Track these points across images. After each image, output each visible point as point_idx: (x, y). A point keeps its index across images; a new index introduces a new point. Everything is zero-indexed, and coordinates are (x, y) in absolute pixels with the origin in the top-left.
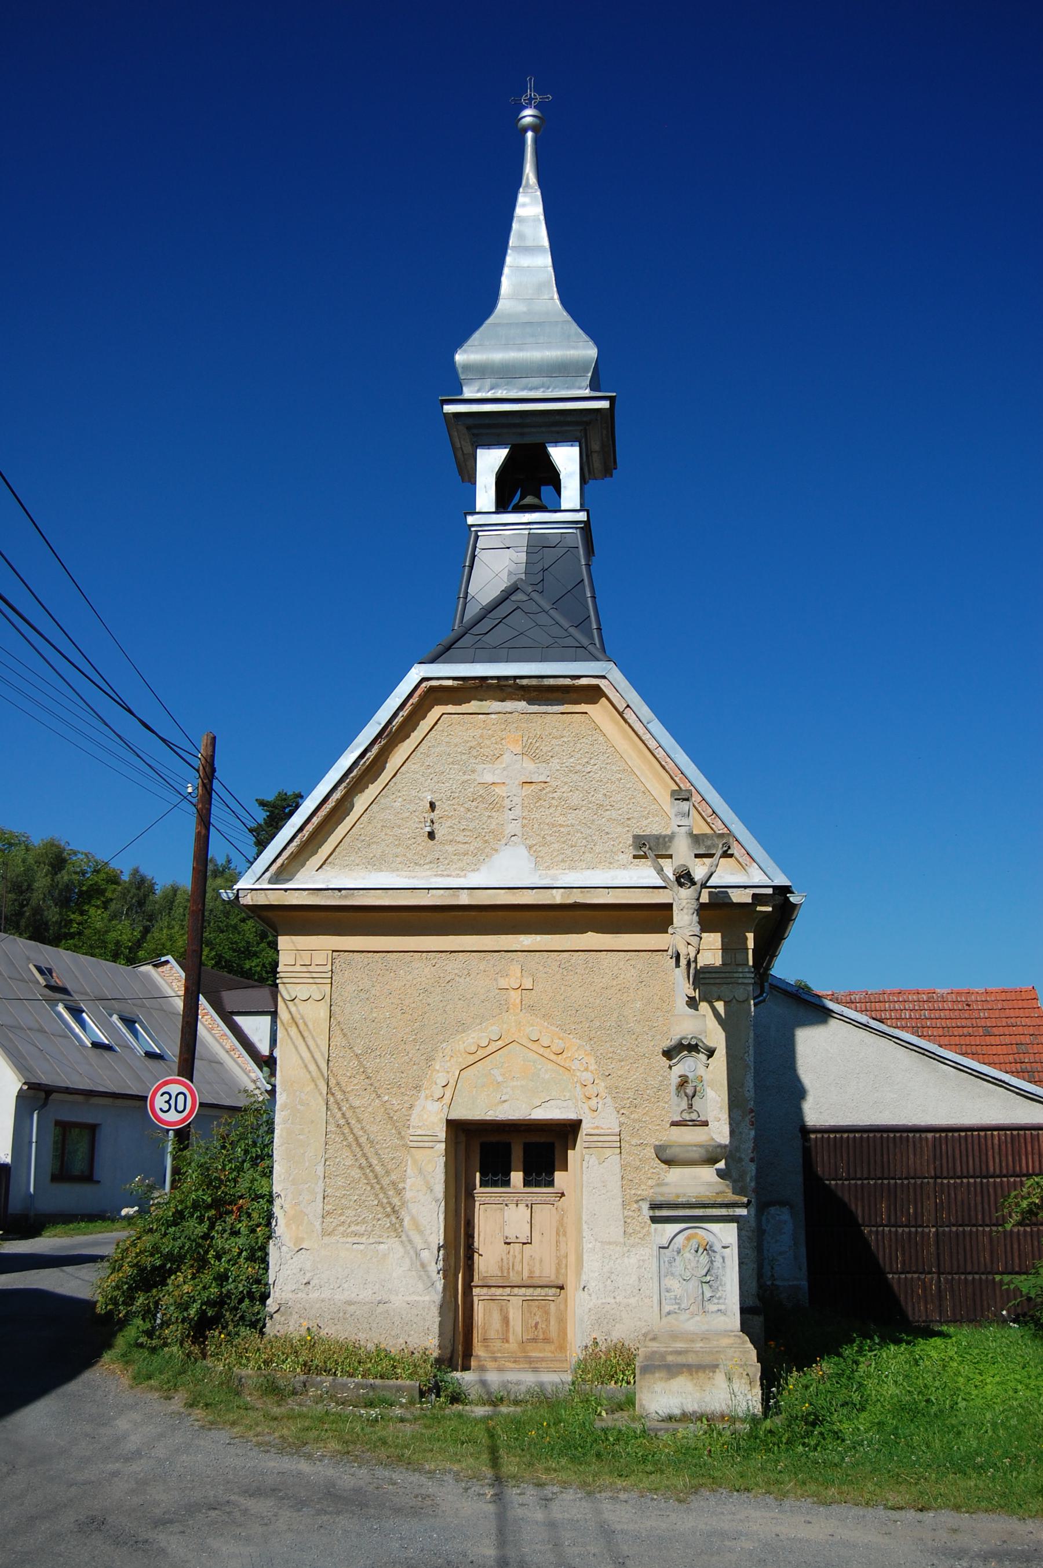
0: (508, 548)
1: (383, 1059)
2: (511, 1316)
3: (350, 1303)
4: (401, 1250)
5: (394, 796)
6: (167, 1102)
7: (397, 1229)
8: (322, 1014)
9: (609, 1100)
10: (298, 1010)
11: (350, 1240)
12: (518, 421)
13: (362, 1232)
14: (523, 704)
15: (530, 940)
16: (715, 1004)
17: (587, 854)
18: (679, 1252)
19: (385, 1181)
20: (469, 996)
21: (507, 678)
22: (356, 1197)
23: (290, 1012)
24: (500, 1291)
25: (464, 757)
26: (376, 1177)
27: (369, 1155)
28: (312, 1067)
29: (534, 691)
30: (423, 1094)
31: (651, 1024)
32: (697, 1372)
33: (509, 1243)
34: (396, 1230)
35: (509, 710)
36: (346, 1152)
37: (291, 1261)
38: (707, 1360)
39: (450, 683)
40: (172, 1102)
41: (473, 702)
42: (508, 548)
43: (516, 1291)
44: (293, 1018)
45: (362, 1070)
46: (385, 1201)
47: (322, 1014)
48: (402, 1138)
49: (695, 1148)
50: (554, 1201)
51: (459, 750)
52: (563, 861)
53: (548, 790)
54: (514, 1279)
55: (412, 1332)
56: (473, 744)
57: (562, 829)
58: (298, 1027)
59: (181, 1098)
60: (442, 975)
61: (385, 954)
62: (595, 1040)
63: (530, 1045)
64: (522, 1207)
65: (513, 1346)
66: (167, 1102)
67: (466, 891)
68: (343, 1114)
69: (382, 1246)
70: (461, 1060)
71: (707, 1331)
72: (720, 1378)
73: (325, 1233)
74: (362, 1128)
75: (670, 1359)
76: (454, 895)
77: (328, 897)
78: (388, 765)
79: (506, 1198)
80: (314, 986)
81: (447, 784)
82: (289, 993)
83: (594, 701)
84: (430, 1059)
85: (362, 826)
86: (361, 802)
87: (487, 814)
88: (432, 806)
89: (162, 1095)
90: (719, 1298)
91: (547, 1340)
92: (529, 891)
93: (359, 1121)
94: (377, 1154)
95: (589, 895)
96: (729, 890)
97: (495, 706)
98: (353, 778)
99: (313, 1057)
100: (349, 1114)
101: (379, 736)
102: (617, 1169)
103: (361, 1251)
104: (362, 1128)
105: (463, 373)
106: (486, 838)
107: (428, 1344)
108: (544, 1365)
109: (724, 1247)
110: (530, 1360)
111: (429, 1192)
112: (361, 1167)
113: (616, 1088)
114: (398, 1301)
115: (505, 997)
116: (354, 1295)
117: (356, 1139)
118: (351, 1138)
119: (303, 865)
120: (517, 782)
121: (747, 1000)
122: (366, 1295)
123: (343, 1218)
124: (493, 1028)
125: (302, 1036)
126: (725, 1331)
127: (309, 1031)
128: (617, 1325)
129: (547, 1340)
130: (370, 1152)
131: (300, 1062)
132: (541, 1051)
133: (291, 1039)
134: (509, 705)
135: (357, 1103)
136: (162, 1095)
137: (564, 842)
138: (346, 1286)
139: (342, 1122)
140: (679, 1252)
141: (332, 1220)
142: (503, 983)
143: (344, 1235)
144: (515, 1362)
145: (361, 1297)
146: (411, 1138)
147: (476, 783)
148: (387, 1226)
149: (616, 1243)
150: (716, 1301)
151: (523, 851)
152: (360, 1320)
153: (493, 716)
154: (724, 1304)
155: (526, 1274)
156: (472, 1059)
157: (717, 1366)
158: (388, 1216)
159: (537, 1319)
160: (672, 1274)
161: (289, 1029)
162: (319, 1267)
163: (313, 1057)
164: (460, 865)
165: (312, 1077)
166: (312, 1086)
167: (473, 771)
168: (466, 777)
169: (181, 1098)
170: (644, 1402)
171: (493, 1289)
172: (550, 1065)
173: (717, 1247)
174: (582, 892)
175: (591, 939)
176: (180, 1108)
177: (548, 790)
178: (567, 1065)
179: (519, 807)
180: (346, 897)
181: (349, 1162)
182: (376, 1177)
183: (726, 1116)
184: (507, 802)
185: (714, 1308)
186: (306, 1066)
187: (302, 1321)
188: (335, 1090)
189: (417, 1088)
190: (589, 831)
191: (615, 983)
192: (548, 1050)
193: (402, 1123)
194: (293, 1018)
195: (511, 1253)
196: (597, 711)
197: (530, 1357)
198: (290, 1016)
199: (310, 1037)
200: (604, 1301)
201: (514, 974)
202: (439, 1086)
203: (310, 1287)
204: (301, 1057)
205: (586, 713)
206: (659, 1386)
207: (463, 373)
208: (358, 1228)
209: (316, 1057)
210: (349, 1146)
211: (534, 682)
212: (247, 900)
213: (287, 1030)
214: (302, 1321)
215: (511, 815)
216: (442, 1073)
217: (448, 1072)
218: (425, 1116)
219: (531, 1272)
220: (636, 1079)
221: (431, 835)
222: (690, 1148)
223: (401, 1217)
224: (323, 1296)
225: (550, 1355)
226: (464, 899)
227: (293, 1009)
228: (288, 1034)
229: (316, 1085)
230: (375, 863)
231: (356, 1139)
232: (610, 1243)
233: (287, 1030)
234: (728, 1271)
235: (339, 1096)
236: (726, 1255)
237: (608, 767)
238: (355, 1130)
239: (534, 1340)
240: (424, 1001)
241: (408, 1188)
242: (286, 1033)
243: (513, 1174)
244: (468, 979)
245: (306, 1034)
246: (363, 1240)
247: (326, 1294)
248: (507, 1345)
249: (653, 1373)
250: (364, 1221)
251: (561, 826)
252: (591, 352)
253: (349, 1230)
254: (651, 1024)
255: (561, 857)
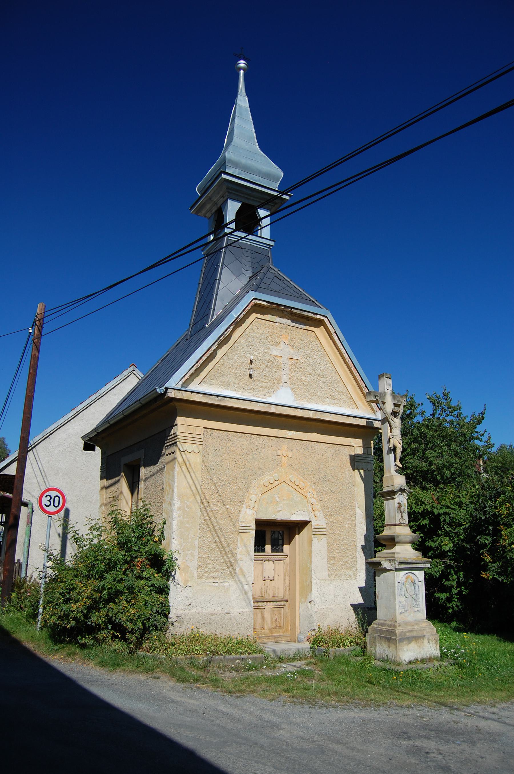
0: (242, 248)
1: (226, 486)
2: (266, 616)
3: (212, 614)
4: (236, 585)
5: (234, 353)
6: (49, 501)
7: (233, 575)
8: (198, 460)
9: (321, 512)
10: (186, 457)
11: (210, 581)
12: (250, 192)
13: (216, 576)
14: (290, 321)
15: (291, 433)
16: (360, 471)
17: (314, 396)
18: (403, 584)
19: (227, 550)
20: (265, 458)
21: (288, 307)
22: (213, 558)
23: (183, 458)
24: (262, 604)
25: (264, 341)
26: (223, 547)
27: (220, 536)
28: (194, 488)
29: (296, 316)
30: (244, 505)
31: (336, 478)
32: (418, 640)
33: (264, 580)
34: (232, 575)
35: (283, 323)
36: (209, 534)
37: (181, 593)
38: (420, 634)
39: (265, 303)
40: (52, 501)
41: (269, 315)
42: (242, 248)
43: (269, 603)
44: (184, 461)
45: (217, 491)
46: (227, 560)
47: (198, 460)
48: (235, 527)
49: (409, 537)
50: (284, 559)
51: (262, 337)
52: (305, 398)
53: (299, 363)
54: (267, 598)
55: (241, 628)
56: (268, 335)
57: (305, 383)
58: (186, 466)
59: (57, 499)
60: (253, 446)
61: (228, 432)
62: (316, 483)
63: (290, 484)
64: (271, 562)
65: (266, 631)
66: (49, 501)
67: (274, 406)
68: (208, 514)
69: (226, 584)
70: (261, 489)
71: (416, 620)
72: (426, 641)
73: (199, 577)
74: (217, 522)
75: (408, 634)
76: (269, 407)
77: (212, 400)
78: (232, 337)
79: (264, 558)
80: (195, 445)
81: (257, 352)
82: (183, 448)
83: (317, 327)
84: (248, 488)
85: (219, 365)
86: (220, 353)
87: (275, 370)
88: (251, 362)
89: (46, 497)
90: (418, 605)
91: (280, 627)
92: (300, 410)
93: (215, 518)
94: (223, 535)
95: (323, 415)
96: (373, 421)
97: (277, 319)
98: (221, 340)
99: (194, 483)
100: (210, 514)
101: (233, 322)
102: (325, 544)
103: (217, 586)
104: (217, 522)
105: (228, 162)
106: (274, 382)
107: (249, 634)
108: (280, 639)
109: (419, 582)
110: (275, 637)
111: (248, 555)
112: (216, 542)
113: (324, 506)
114: (234, 612)
115: (280, 460)
116: (213, 610)
117: (214, 527)
118: (211, 527)
119: (193, 381)
120: (287, 357)
121: (371, 471)
122: (218, 609)
123: (207, 569)
124: (276, 474)
125: (189, 471)
126: (422, 620)
127: (192, 468)
128: (327, 618)
129: (280, 627)
130: (220, 534)
131: (187, 485)
132: (295, 487)
133: (183, 472)
134: (284, 321)
135: (214, 508)
136: (46, 497)
137: (305, 389)
138: (208, 605)
139: (207, 518)
140: (403, 584)
141: (201, 570)
142: (280, 453)
143: (208, 578)
144: (268, 639)
145: (216, 611)
146: (240, 528)
147: (270, 354)
148: (228, 573)
149: (326, 580)
150: (417, 606)
151: (290, 391)
152: (218, 624)
153: (276, 324)
154: (419, 607)
155: (271, 595)
156: (266, 489)
157: (424, 636)
158: (228, 568)
159: (277, 617)
160: (402, 595)
161: (182, 467)
162: (196, 596)
163: (194, 483)
164: (262, 393)
165: (193, 493)
166: (193, 498)
167: (268, 348)
168: (265, 351)
169: (57, 499)
170: (400, 656)
171: (259, 603)
172: (299, 494)
173: (417, 582)
174: (320, 414)
175: (315, 436)
176: (56, 504)
177: (299, 363)
178: (305, 495)
179: (287, 369)
180: (220, 400)
181: (210, 539)
182: (223, 547)
183: (365, 521)
184: (283, 366)
185: (416, 609)
186: (190, 487)
187: (189, 625)
188: (204, 501)
189: (242, 502)
190: (315, 386)
191: (323, 458)
192: (298, 486)
193: (235, 520)
194: (184, 461)
195: (266, 585)
196: (320, 332)
197: (274, 636)
198: (182, 460)
199: (192, 472)
200: (321, 607)
201: (285, 449)
202: (253, 502)
203: (191, 606)
204: (188, 482)
205: (313, 331)
206: (405, 648)
207: (228, 162)
208: (214, 574)
209: (195, 483)
210: (210, 531)
211: (299, 312)
212: (172, 394)
213: (181, 467)
214: (189, 625)
215: (284, 372)
216: (254, 495)
217: (256, 495)
218: (246, 517)
219: (274, 594)
220: (331, 503)
221: (251, 376)
222: (407, 536)
223: (234, 568)
224: (198, 611)
225: (282, 634)
226: (273, 410)
227: (184, 456)
228: (181, 469)
229: (195, 498)
230: (226, 385)
231: (214, 527)
232: (323, 580)
233: (181, 467)
234: (420, 592)
235: (206, 504)
236: (419, 585)
237: (322, 358)
238: (213, 523)
239: (275, 627)
240: (245, 458)
241: (238, 553)
242: (180, 469)
243: (266, 546)
244: (264, 449)
245: (190, 470)
246: (217, 580)
247: (199, 610)
248: (264, 631)
249: (403, 642)
250: (217, 571)
251: (304, 381)
252: (282, 174)
253: (210, 575)
254: (336, 478)
255: (304, 396)
